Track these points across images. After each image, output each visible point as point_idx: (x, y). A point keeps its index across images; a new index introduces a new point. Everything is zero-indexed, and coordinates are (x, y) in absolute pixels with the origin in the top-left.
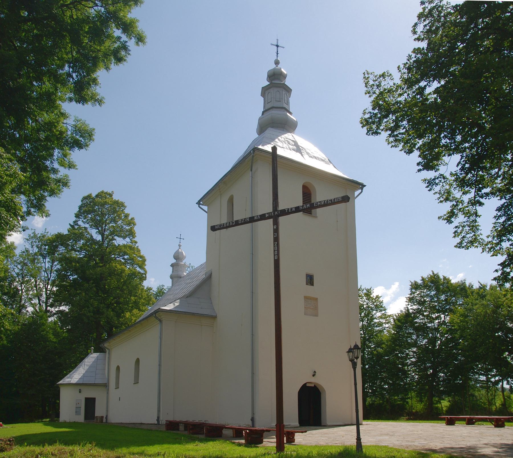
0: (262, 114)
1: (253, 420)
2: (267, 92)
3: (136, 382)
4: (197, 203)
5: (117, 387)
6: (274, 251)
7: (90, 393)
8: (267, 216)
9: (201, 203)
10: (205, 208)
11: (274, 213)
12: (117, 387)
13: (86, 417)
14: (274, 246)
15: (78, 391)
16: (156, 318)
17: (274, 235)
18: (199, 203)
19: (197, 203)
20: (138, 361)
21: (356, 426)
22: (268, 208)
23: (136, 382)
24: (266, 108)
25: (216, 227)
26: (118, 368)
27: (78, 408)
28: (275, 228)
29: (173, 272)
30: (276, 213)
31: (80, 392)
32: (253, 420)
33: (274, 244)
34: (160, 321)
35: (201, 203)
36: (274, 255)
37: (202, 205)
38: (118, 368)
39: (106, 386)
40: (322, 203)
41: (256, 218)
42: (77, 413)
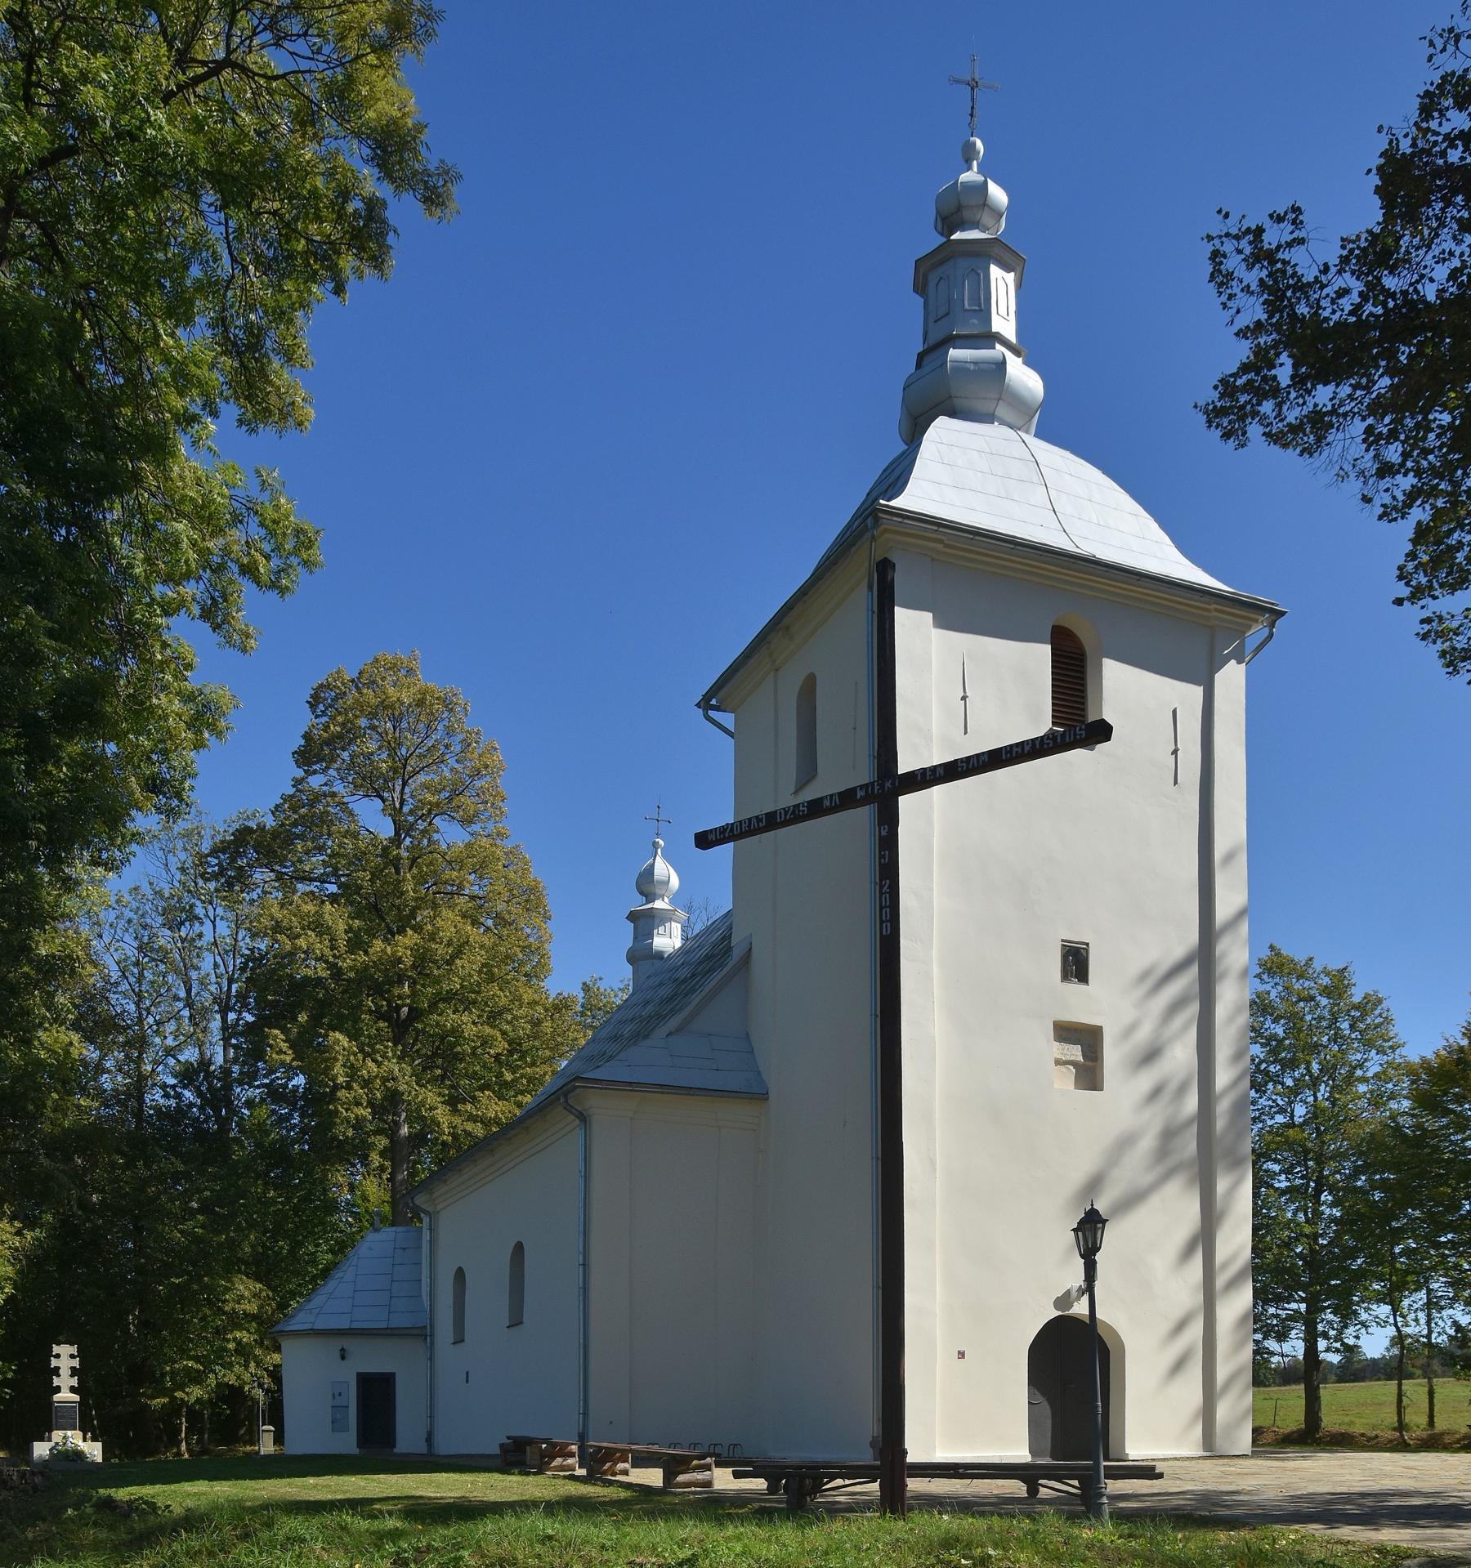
0: (919, 365)
1: (429, 1440)
2: (933, 278)
3: (516, 1322)
4: (698, 705)
5: (459, 1340)
6: (881, 908)
7: (374, 1359)
8: (860, 794)
9: (714, 702)
10: (727, 719)
11: (882, 786)
12: (459, 1340)
13: (364, 1439)
14: (881, 894)
15: (337, 1354)
16: (569, 1108)
17: (881, 857)
18: (705, 704)
19: (698, 705)
20: (519, 1248)
21: (915, 1454)
22: (861, 774)
23: (516, 1322)
24: (932, 341)
25: (712, 837)
26: (460, 1274)
27: (339, 1409)
28: (884, 833)
29: (635, 938)
30: (888, 784)
31: (343, 1358)
32: (429, 1440)
33: (881, 887)
34: (583, 1118)
35: (714, 702)
36: (882, 922)
37: (717, 708)
38: (460, 1274)
39: (422, 1334)
40: (1027, 748)
41: (827, 803)
42: (337, 1425)
